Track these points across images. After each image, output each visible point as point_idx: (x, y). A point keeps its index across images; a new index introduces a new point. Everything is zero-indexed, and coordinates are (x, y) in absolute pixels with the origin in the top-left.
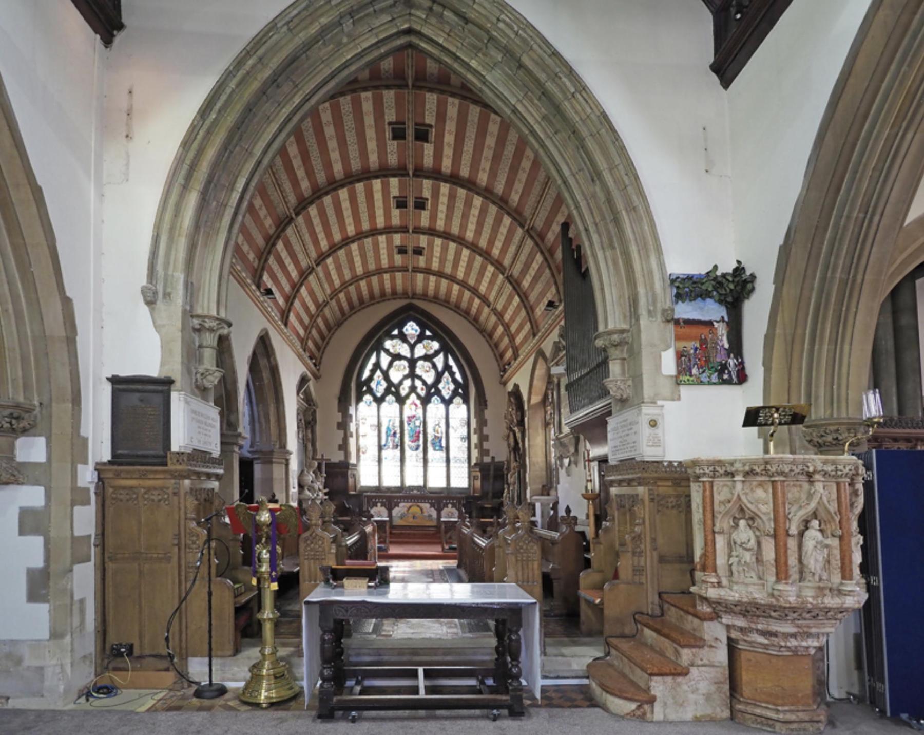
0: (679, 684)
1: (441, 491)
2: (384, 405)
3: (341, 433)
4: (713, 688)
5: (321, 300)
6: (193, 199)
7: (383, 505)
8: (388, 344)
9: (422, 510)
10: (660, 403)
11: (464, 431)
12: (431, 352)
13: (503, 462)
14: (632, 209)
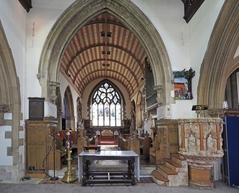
0: (175, 177)
1: (114, 127)
4: (184, 178)
6: (50, 52)
8: (100, 89)
10: (170, 104)
12: (111, 91)
14: (163, 54)
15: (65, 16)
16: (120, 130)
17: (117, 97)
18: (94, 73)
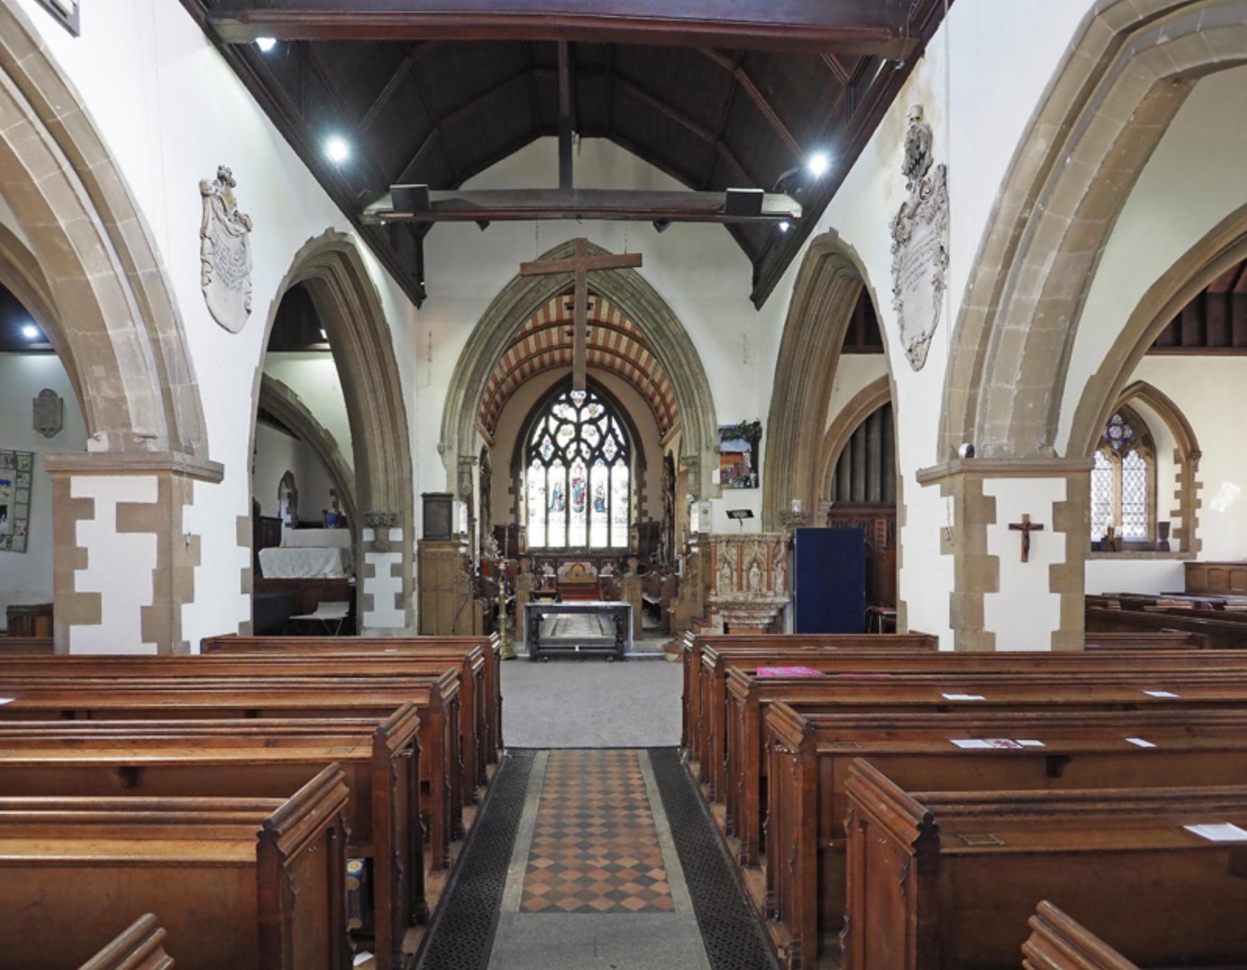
1: (602, 550)
2: (552, 469)
3: (513, 496)
5: (499, 379)
6: (463, 393)
7: (550, 564)
9: (584, 568)
10: (711, 500)
11: (625, 492)
12: (596, 415)
13: (658, 523)
14: (698, 387)
15: (492, 313)
16: (618, 558)
17: (615, 437)
18: (531, 339)
